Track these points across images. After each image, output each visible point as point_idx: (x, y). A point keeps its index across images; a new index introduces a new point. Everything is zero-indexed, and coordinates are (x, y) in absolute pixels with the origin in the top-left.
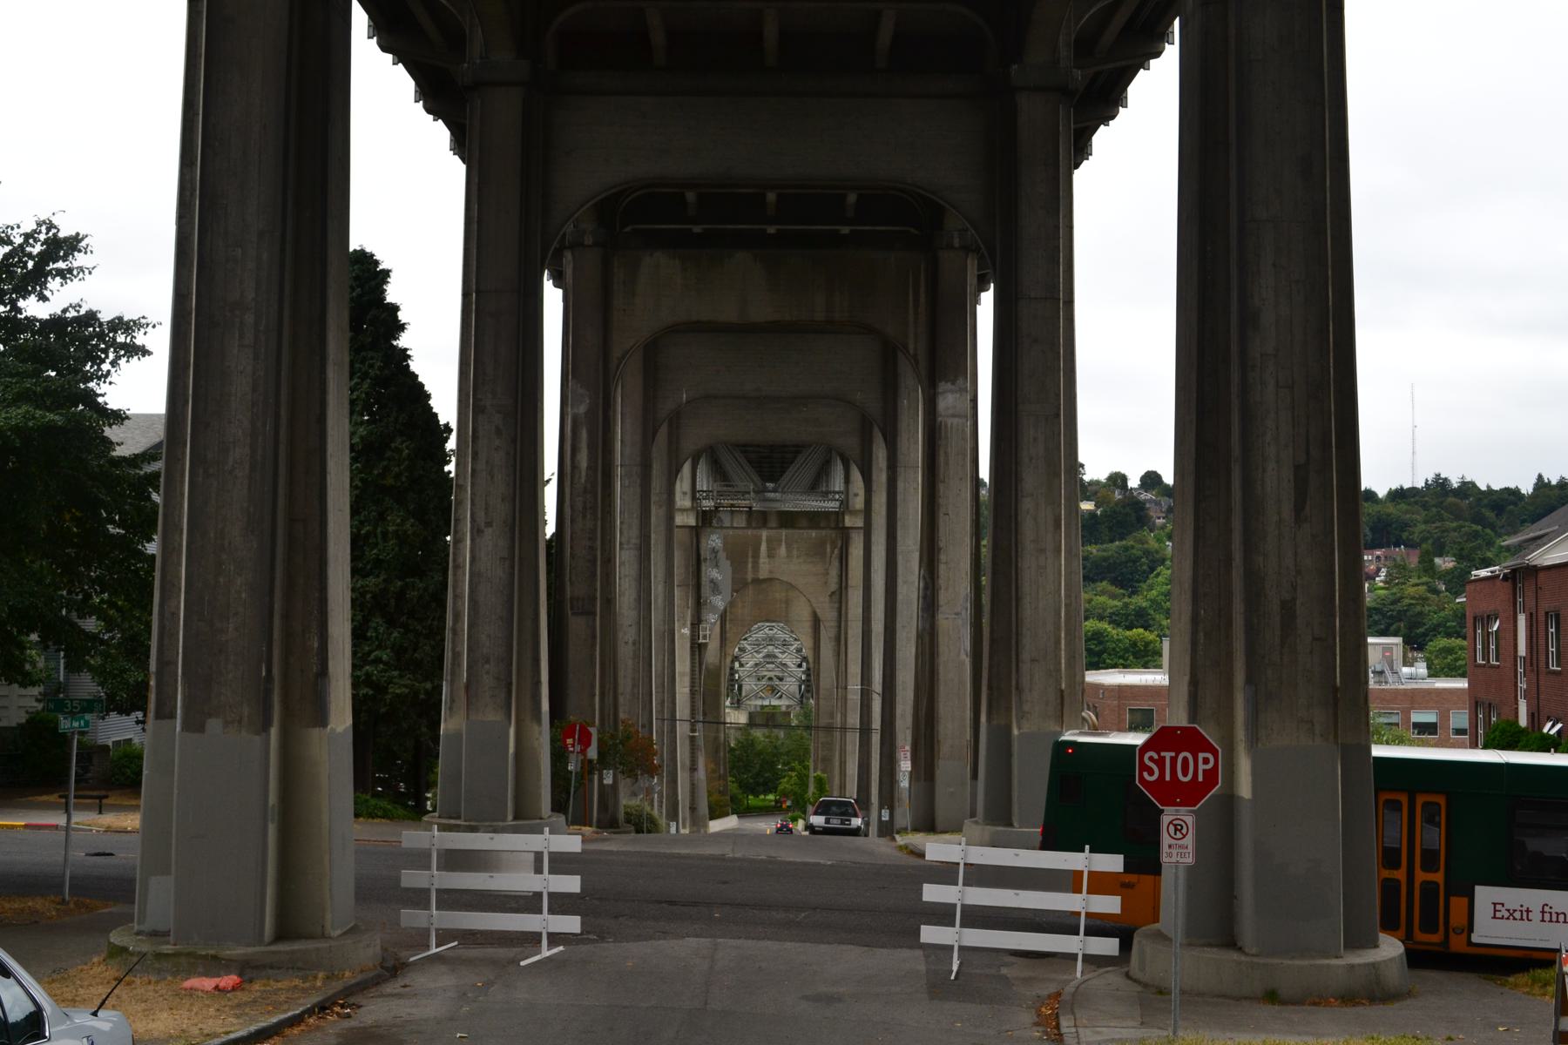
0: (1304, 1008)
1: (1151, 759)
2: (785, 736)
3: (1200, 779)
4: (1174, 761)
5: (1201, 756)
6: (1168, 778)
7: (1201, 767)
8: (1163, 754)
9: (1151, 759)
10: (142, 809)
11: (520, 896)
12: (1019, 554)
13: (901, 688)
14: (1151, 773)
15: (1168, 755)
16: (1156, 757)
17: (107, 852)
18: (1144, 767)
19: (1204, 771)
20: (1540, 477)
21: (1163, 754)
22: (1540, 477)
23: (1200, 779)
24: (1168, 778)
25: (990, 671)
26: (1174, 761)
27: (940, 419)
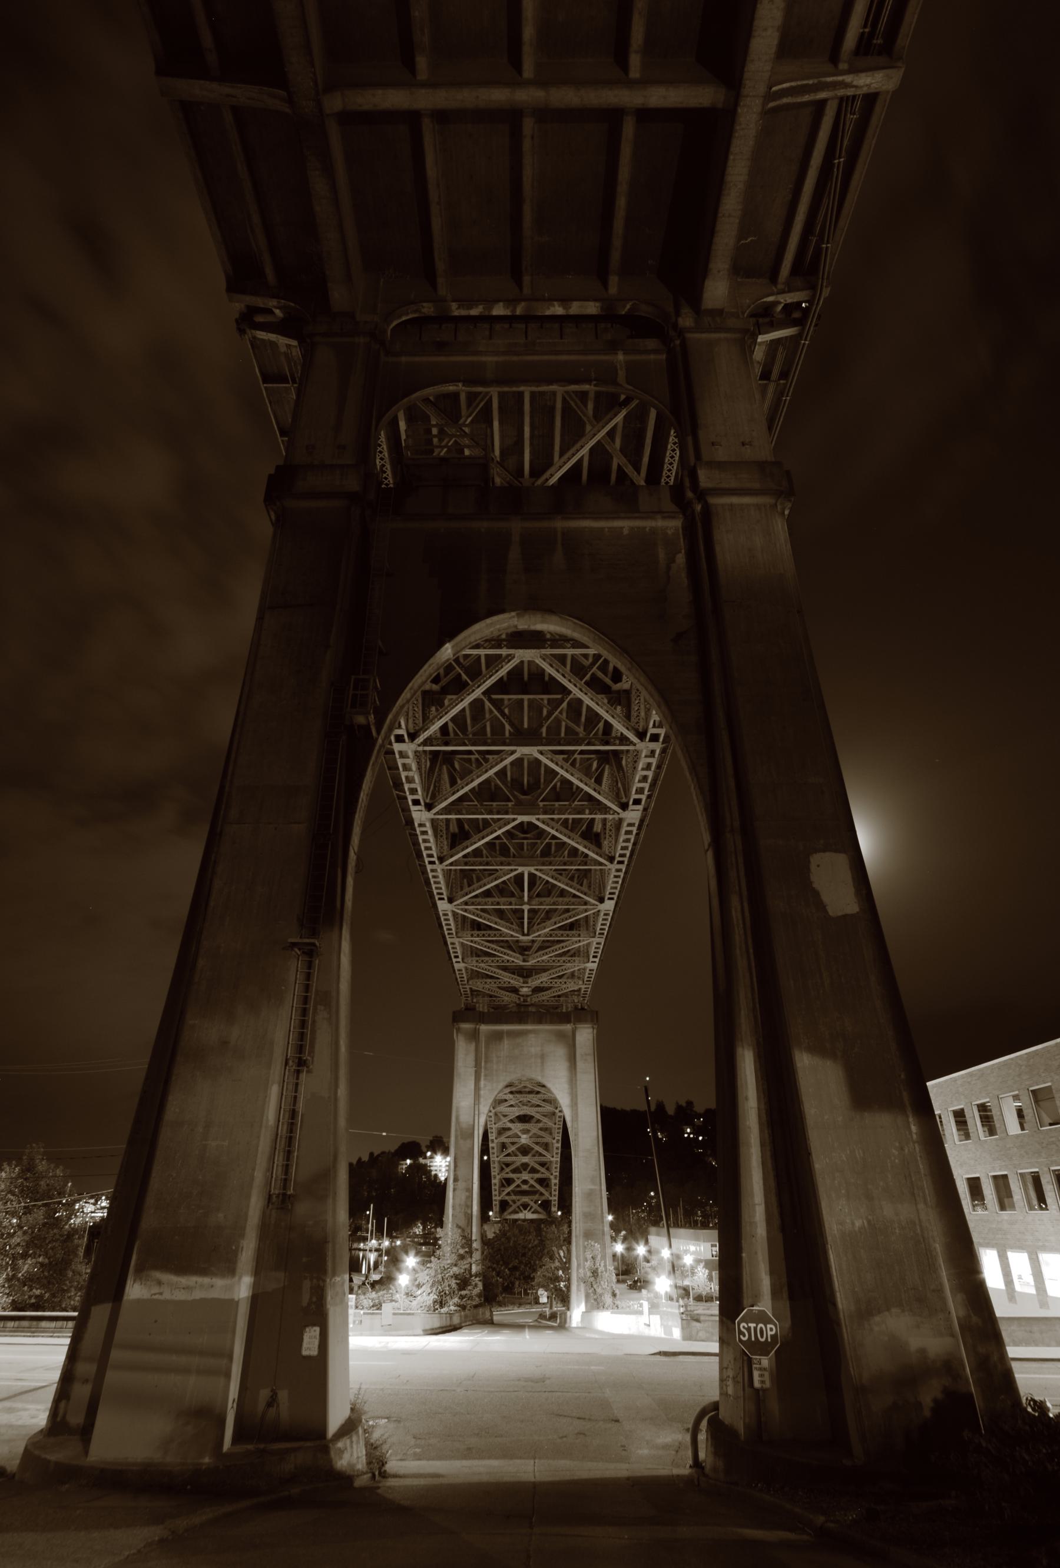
0: (534, 977)
1: (744, 1327)
2: (783, 380)
3: (769, 1340)
4: (755, 1329)
5: (769, 1326)
6: (753, 1339)
7: (770, 1333)
8: (750, 1325)
9: (744, 1327)
10: (448, 1234)
11: (477, 1459)
12: (282, 1144)
13: (625, 1466)
14: (744, 1336)
15: (752, 1325)
16: (746, 1326)
17: (370, 1316)
18: (741, 1333)
19: (771, 1335)
20: (677, 1103)
21: (750, 1325)
22: (677, 1103)
23: (769, 1340)
24: (753, 1339)
25: (481, 775)
26: (755, 1329)
27: (380, 92)
